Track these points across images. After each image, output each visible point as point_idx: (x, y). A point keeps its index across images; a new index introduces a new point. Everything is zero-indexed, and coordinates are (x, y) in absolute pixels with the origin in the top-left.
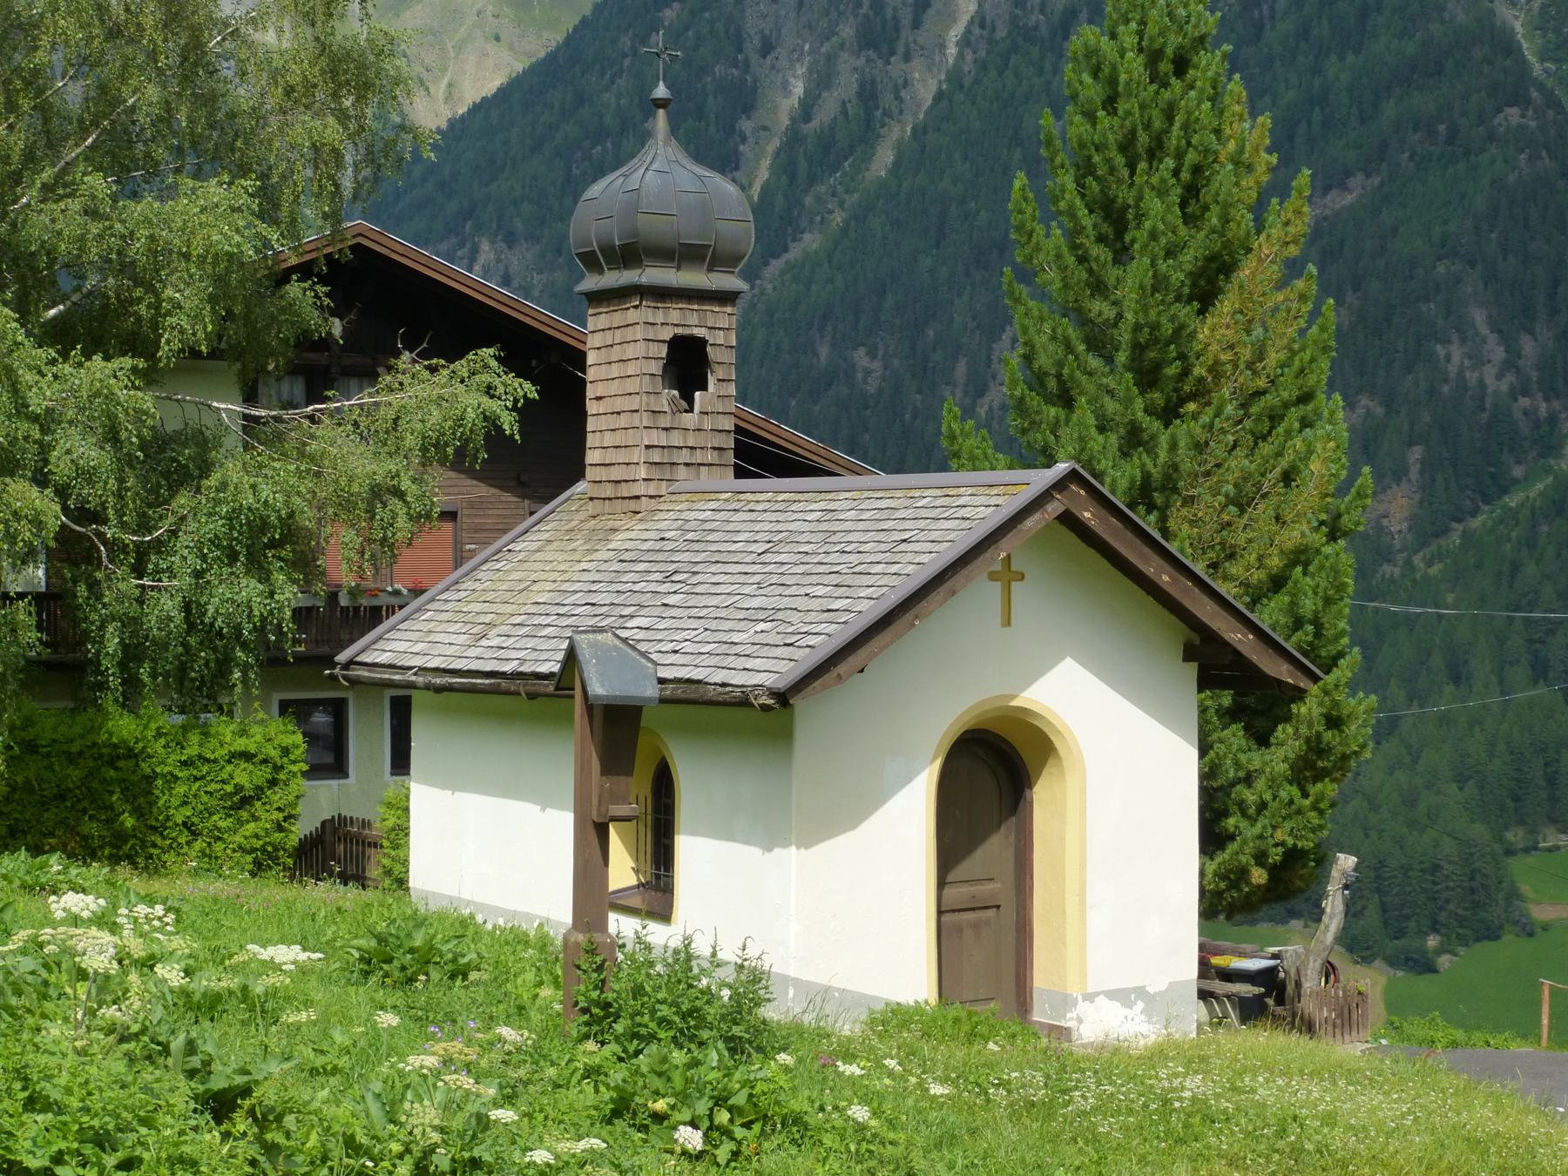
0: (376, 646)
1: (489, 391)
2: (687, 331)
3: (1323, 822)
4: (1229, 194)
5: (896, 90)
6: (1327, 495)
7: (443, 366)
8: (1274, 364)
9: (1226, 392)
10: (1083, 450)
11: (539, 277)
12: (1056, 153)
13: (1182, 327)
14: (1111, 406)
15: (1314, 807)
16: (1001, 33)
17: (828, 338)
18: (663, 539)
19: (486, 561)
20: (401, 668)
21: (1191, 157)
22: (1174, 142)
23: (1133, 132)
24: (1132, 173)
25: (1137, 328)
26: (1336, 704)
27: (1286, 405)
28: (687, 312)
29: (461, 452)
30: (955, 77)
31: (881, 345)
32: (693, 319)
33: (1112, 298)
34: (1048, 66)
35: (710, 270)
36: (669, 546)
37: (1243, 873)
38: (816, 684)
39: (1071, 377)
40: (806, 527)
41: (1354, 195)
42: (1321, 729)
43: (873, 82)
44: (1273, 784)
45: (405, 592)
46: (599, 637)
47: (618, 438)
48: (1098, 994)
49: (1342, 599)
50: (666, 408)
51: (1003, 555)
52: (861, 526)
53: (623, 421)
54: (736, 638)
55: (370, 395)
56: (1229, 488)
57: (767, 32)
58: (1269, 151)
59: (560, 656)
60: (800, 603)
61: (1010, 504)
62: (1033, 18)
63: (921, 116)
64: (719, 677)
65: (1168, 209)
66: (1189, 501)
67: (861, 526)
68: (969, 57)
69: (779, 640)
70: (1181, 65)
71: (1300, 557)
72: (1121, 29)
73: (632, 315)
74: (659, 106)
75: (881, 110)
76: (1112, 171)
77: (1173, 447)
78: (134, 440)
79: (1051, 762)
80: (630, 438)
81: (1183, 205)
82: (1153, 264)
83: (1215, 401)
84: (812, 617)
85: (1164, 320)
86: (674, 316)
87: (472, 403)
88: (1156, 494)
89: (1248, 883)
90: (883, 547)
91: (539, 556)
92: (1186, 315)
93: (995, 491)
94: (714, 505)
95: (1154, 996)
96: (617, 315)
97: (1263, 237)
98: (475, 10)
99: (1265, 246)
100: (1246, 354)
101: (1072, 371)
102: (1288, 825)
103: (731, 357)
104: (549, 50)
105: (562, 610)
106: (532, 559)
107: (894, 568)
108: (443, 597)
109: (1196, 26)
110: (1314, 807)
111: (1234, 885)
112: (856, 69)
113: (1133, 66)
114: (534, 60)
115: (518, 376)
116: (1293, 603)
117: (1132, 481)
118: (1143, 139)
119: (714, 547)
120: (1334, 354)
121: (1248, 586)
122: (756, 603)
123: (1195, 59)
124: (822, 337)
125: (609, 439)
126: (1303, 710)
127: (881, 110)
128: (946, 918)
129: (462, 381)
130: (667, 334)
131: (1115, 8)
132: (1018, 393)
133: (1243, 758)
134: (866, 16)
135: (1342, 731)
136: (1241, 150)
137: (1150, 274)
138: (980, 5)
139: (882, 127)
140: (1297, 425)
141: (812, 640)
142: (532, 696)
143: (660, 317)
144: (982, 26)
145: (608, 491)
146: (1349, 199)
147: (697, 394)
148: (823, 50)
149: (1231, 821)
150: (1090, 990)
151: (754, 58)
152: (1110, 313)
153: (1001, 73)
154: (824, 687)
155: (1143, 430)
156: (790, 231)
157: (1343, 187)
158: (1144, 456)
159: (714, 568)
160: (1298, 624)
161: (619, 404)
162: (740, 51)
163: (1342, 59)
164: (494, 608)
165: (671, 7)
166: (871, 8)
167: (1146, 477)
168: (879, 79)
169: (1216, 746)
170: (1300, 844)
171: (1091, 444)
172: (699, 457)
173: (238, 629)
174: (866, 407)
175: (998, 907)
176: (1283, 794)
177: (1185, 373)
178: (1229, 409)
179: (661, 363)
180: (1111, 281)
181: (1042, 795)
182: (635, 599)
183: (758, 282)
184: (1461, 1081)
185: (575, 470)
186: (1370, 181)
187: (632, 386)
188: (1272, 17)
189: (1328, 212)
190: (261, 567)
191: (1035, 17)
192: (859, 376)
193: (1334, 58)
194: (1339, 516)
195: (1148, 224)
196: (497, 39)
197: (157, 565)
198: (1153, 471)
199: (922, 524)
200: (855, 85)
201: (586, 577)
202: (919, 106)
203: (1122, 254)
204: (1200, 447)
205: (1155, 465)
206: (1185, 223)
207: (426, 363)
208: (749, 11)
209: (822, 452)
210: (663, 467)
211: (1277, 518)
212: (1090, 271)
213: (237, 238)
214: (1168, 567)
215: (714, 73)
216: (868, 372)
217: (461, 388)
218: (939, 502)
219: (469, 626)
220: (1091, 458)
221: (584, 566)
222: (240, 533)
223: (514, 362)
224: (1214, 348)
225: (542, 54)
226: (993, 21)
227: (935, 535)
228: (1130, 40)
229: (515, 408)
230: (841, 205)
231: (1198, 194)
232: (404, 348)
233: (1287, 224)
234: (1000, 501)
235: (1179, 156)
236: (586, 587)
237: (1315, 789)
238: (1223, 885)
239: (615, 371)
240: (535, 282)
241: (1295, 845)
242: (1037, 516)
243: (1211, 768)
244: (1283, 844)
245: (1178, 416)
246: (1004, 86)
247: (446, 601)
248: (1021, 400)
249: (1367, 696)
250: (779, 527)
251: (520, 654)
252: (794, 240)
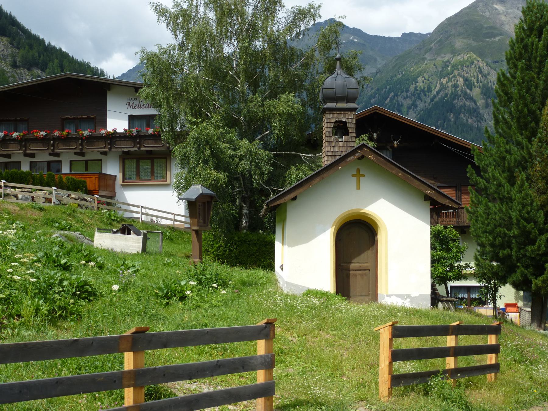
2: (340, 120)
32: (342, 116)
35: (347, 103)
48: (392, 295)
74: (337, 60)
86: (336, 116)
95: (414, 297)
130: (334, 120)
143: (331, 116)
150: (389, 294)
175: (369, 270)
184: (103, 248)
214: (400, 171)
242: (352, 157)
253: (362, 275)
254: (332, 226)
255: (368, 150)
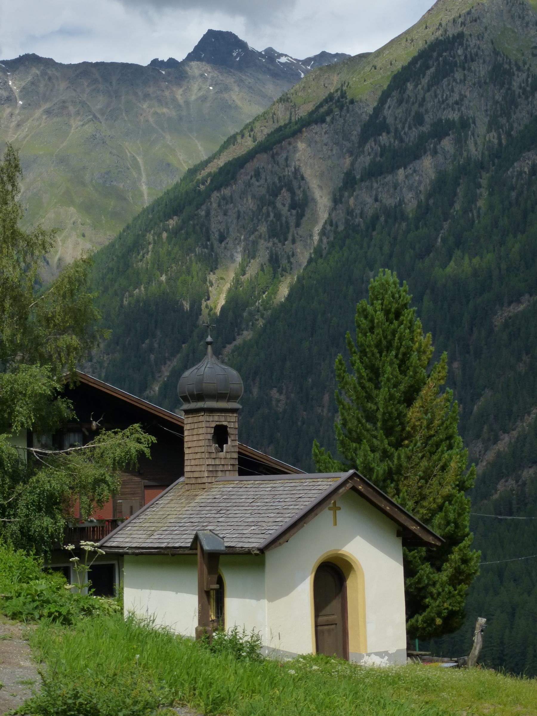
0: (111, 540)
1: (138, 441)
2: (221, 423)
3: (462, 600)
4: (416, 363)
5: (289, 258)
6: (458, 475)
7: (120, 432)
8: (436, 425)
9: (418, 438)
10: (365, 459)
11: (107, 357)
12: (352, 347)
13: (401, 412)
14: (376, 442)
15: (459, 594)
16: (341, 228)
17: (257, 384)
18: (215, 498)
19: (148, 508)
20: (122, 547)
21: (402, 350)
22: (396, 344)
23: (380, 341)
24: (381, 356)
25: (384, 414)
26: (465, 555)
27: (442, 441)
28: (221, 417)
29: (128, 464)
30: (318, 251)
31: (284, 387)
32: (223, 419)
33: (375, 401)
34: (365, 245)
35: (228, 401)
36: (218, 501)
37: (433, 620)
38: (273, 546)
39: (361, 432)
40: (266, 493)
41: (524, 305)
42: (459, 564)
43: (276, 254)
44: (443, 586)
45: (95, 521)
46: (205, 532)
47: (197, 462)
48: (371, 653)
49: (464, 513)
50: (214, 451)
51: (332, 502)
52: (285, 492)
53: (198, 456)
54: (245, 532)
55: (92, 444)
56: (421, 473)
57: (222, 230)
58: (432, 345)
59: (193, 536)
60: (266, 519)
61: (334, 484)
62: (357, 220)
63: (302, 271)
64: (240, 545)
65: (394, 369)
66: (406, 478)
67: (285, 492)
68: (325, 240)
69: (259, 532)
70: (398, 315)
71: (449, 498)
72: (375, 302)
73: (201, 418)
75: (281, 268)
76: (373, 354)
77: (399, 458)
78: (9, 465)
79: (352, 572)
80: (201, 462)
81: (400, 367)
82: (389, 391)
83: (414, 441)
84: (270, 524)
85: (394, 410)
86: (216, 418)
87: (133, 446)
88: (394, 476)
89: (435, 624)
90: (293, 500)
91: (169, 505)
92: (402, 409)
93: (330, 480)
94: (232, 486)
96: (196, 418)
97: (430, 379)
98: (72, 221)
99: (430, 383)
100: (425, 423)
101: (361, 430)
102: (449, 602)
103: (236, 432)
104: (111, 241)
105: (181, 525)
106: (166, 506)
107: (297, 507)
108: (134, 521)
109: (403, 300)
110: (459, 594)
111: (429, 625)
112: (267, 248)
113: (380, 316)
114: (103, 246)
115: (149, 434)
116: (446, 515)
117: (384, 470)
118: (384, 343)
119: (234, 501)
120: (459, 421)
121: (430, 510)
122: (250, 520)
123: (403, 312)
124: (254, 384)
125: (193, 462)
126: (453, 557)
127: (281, 268)
128: (319, 628)
129: (128, 437)
130: (214, 425)
131: (372, 293)
132: (341, 438)
133: (431, 576)
134: (272, 221)
135: (468, 565)
136: (420, 346)
137: (388, 394)
138: (329, 215)
139: (282, 277)
140: (445, 448)
141: (271, 532)
142: (173, 555)
143: (211, 419)
144: (331, 225)
145: (193, 481)
146: (522, 307)
147: (225, 445)
148: (251, 239)
149: (427, 600)
150: (369, 652)
151: (216, 244)
152: (374, 407)
153: (341, 248)
154: (276, 547)
155: (387, 452)
156: (236, 330)
157: (519, 302)
158: (389, 461)
159: (235, 508)
160: (448, 523)
161: (197, 450)
162: (209, 240)
163: (515, 236)
164: (154, 525)
165: (172, 219)
166: (274, 217)
167: (390, 469)
168: (279, 253)
169: (420, 571)
170: (454, 609)
171: (369, 457)
172: (226, 468)
173: (42, 537)
174: (278, 419)
175: (336, 624)
176: (446, 589)
177: (403, 429)
178: (419, 444)
179: (212, 435)
180: (374, 396)
181: (350, 583)
182: (207, 520)
183: (220, 356)
185: (181, 473)
186: (532, 298)
187: (201, 443)
188: (479, 217)
189: (511, 314)
190: (51, 513)
191: (358, 220)
192: (274, 403)
193: (511, 236)
194: (464, 482)
195: (386, 376)
196: (84, 236)
197: (9, 512)
198: (392, 467)
199: (305, 491)
200: (268, 256)
201: (188, 512)
202: (300, 266)
203: (377, 387)
204: (409, 458)
205: (393, 465)
206: (401, 374)
207: (113, 430)
208: (212, 220)
209: (265, 457)
210: (213, 472)
211: (440, 484)
212: (366, 392)
213: (44, 388)
214: (388, 504)
215: (196, 252)
216: (278, 401)
217: (128, 440)
218: (311, 484)
219: (146, 532)
220: (369, 463)
221: (186, 509)
222: (43, 500)
223: (146, 429)
224: (413, 420)
225: (107, 243)
226: (336, 223)
227: (310, 495)
228: (378, 307)
229: (148, 447)
230: (262, 317)
231: (405, 363)
232: (93, 420)
233: (439, 372)
234: (331, 483)
235: (398, 349)
236: (188, 516)
237: (459, 587)
238: (425, 625)
239: (195, 438)
240: (105, 359)
241: (452, 609)
242: (344, 488)
243: (419, 580)
244: (447, 609)
245: (401, 446)
246: (343, 255)
247: (135, 523)
248: (343, 440)
249: (477, 551)
250: (257, 493)
251: (167, 541)
252: (239, 334)
253: (329, 631)
254: (311, 574)
255: (358, 480)
